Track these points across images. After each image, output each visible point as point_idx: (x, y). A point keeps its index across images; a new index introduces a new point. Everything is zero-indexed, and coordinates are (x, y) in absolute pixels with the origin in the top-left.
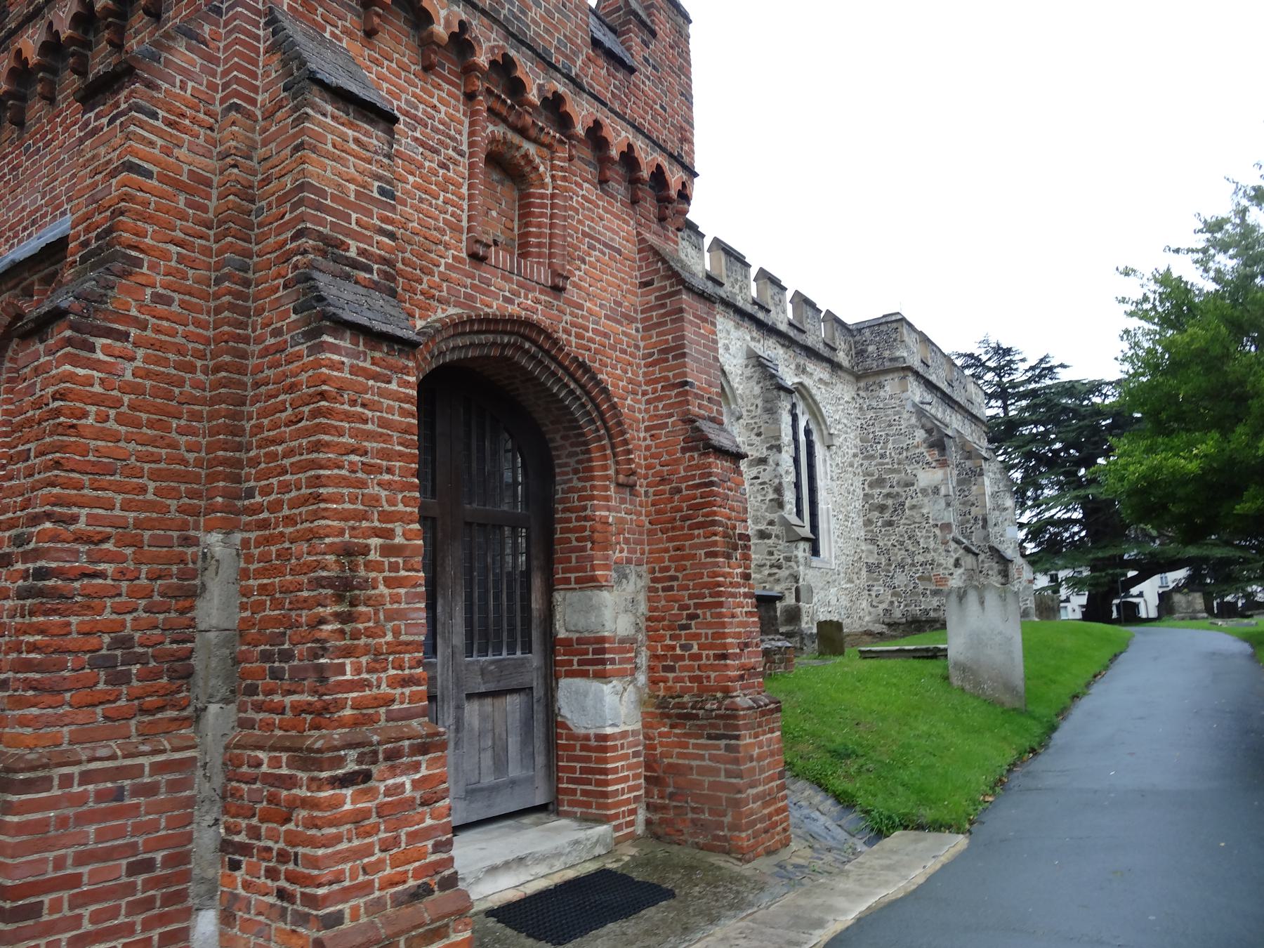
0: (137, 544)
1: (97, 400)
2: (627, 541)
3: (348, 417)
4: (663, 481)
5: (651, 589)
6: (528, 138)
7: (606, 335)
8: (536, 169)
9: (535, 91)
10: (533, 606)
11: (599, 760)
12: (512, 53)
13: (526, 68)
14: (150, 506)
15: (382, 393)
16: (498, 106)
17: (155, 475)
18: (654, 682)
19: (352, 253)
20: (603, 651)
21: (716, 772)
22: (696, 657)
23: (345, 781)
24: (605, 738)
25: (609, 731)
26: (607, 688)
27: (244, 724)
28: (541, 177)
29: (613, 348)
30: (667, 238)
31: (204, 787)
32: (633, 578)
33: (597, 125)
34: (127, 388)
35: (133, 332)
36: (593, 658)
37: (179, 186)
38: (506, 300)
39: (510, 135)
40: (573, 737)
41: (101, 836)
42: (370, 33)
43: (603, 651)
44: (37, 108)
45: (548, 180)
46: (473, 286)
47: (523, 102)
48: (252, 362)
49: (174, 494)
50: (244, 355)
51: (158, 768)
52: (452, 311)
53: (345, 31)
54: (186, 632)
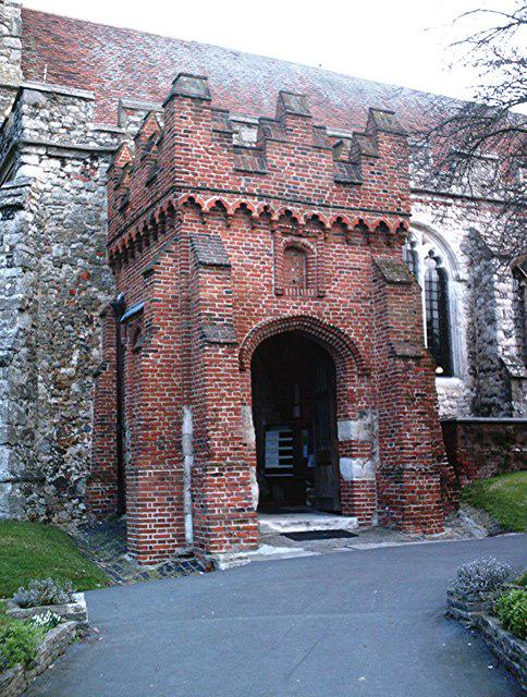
0: (163, 410)
1: (152, 371)
2: (365, 399)
3: (214, 370)
4: (383, 371)
5: (380, 420)
6: (301, 236)
7: (350, 310)
8: (309, 248)
9: (302, 219)
10: (253, 430)
11: (350, 496)
12: (289, 208)
13: (295, 209)
14: (166, 399)
15: (226, 361)
16: (286, 230)
17: (168, 390)
18: (382, 459)
19: (217, 316)
20: (351, 446)
21: (397, 497)
22: (394, 449)
23: (216, 475)
24: (353, 482)
25: (355, 479)
26: (354, 462)
27: (195, 461)
28: (312, 250)
29: (356, 315)
30: (394, 252)
31: (187, 479)
32: (369, 415)
33: (339, 219)
34: (159, 366)
35: (159, 350)
36: (349, 449)
37: (169, 302)
38: (294, 308)
39: (295, 239)
40: (345, 482)
41: (159, 489)
42: (228, 226)
43: (351, 446)
44: (137, 254)
45: (315, 251)
46: (278, 307)
47: (297, 225)
48: (193, 353)
49: (173, 395)
50: (190, 351)
51: (173, 473)
52: (269, 318)
53: (219, 229)
54: (179, 435)
